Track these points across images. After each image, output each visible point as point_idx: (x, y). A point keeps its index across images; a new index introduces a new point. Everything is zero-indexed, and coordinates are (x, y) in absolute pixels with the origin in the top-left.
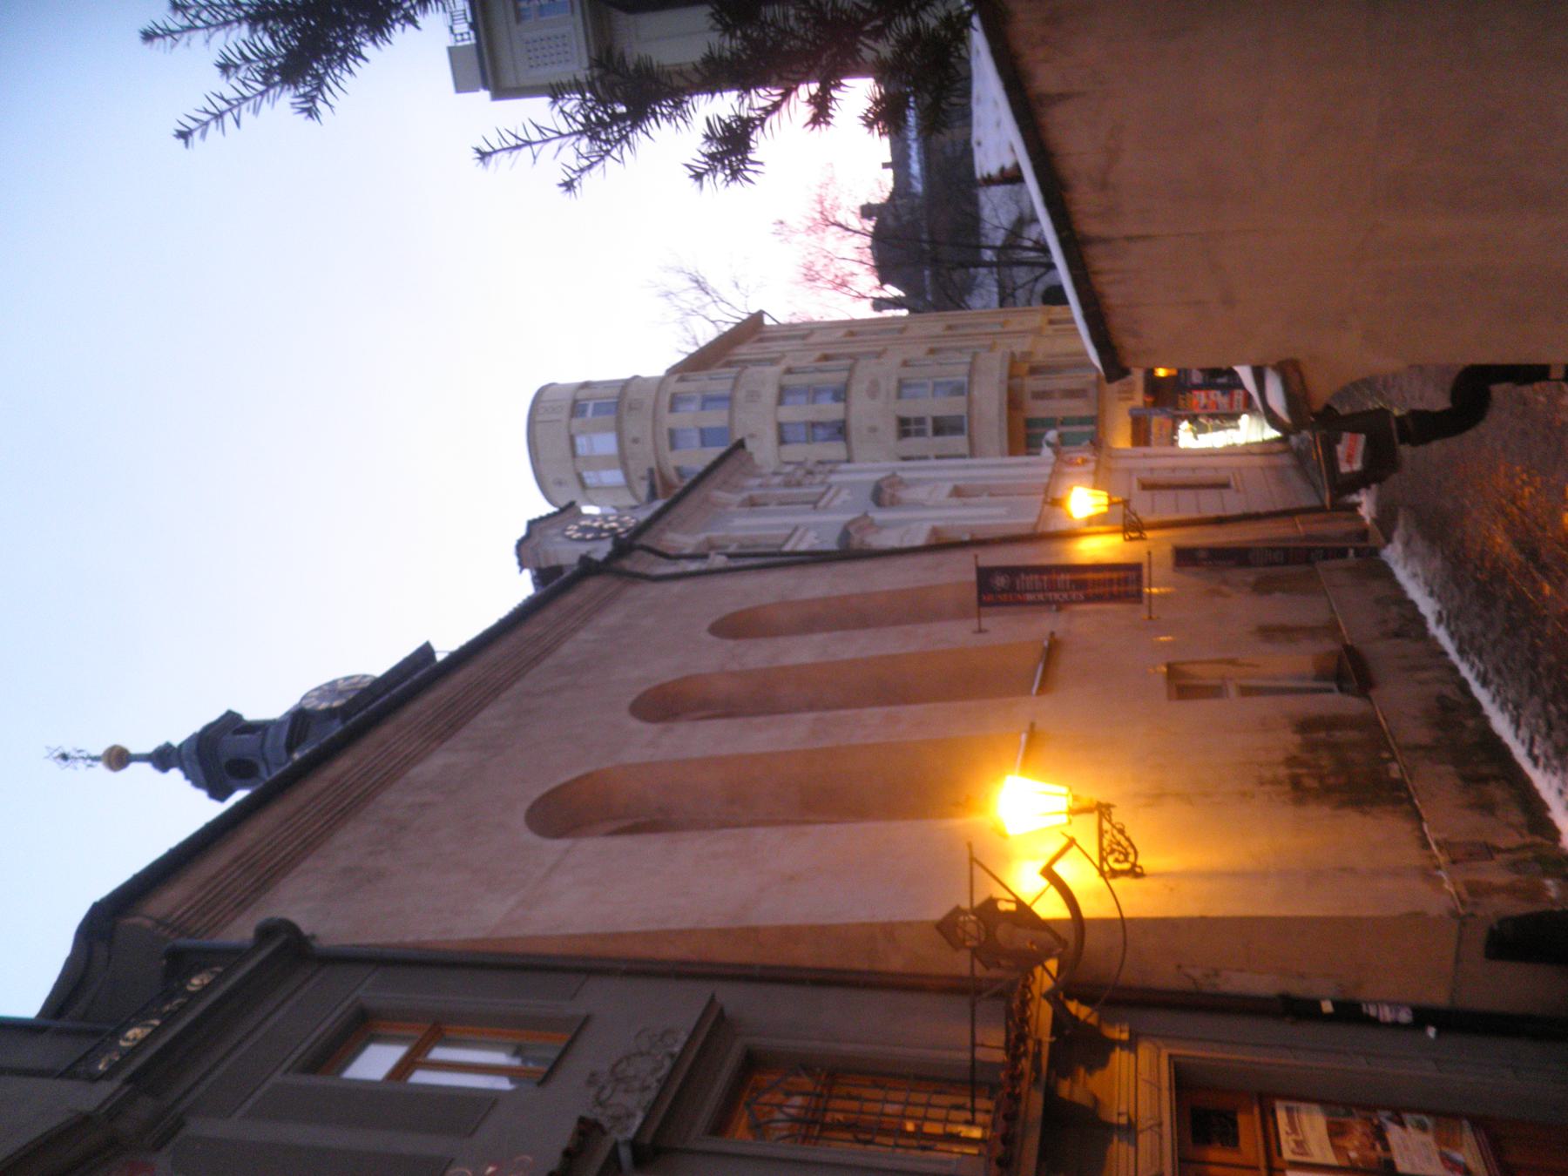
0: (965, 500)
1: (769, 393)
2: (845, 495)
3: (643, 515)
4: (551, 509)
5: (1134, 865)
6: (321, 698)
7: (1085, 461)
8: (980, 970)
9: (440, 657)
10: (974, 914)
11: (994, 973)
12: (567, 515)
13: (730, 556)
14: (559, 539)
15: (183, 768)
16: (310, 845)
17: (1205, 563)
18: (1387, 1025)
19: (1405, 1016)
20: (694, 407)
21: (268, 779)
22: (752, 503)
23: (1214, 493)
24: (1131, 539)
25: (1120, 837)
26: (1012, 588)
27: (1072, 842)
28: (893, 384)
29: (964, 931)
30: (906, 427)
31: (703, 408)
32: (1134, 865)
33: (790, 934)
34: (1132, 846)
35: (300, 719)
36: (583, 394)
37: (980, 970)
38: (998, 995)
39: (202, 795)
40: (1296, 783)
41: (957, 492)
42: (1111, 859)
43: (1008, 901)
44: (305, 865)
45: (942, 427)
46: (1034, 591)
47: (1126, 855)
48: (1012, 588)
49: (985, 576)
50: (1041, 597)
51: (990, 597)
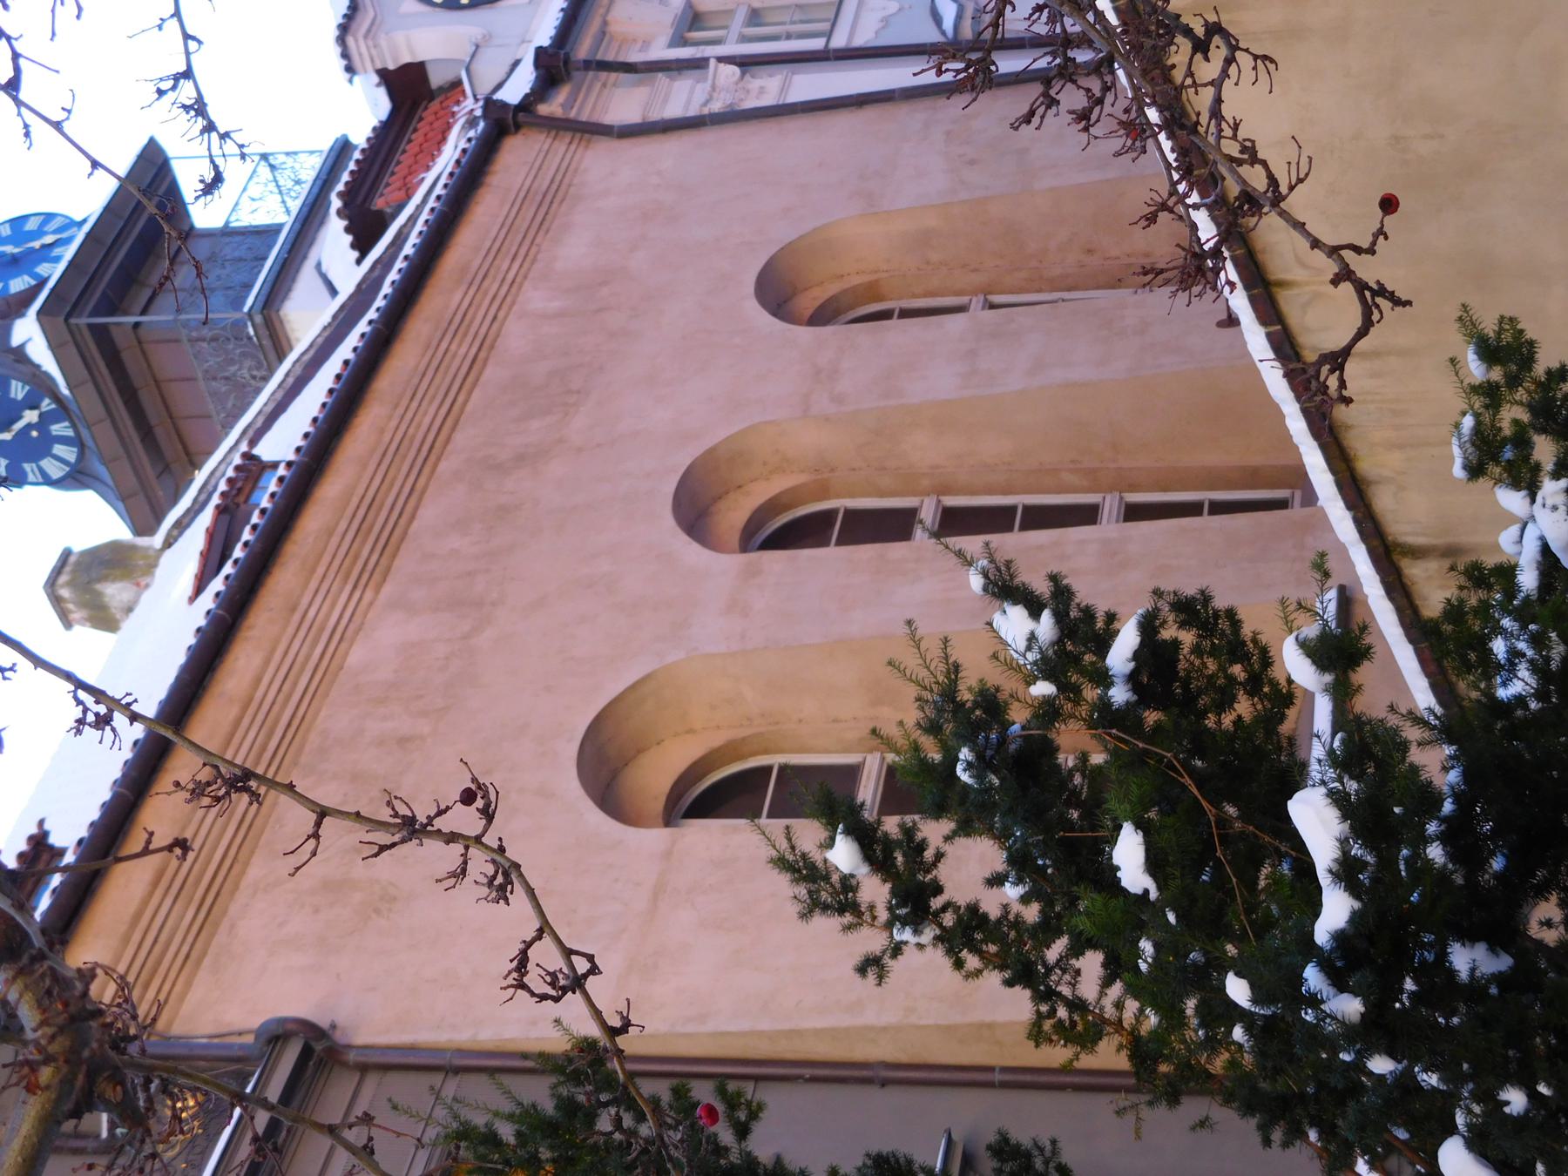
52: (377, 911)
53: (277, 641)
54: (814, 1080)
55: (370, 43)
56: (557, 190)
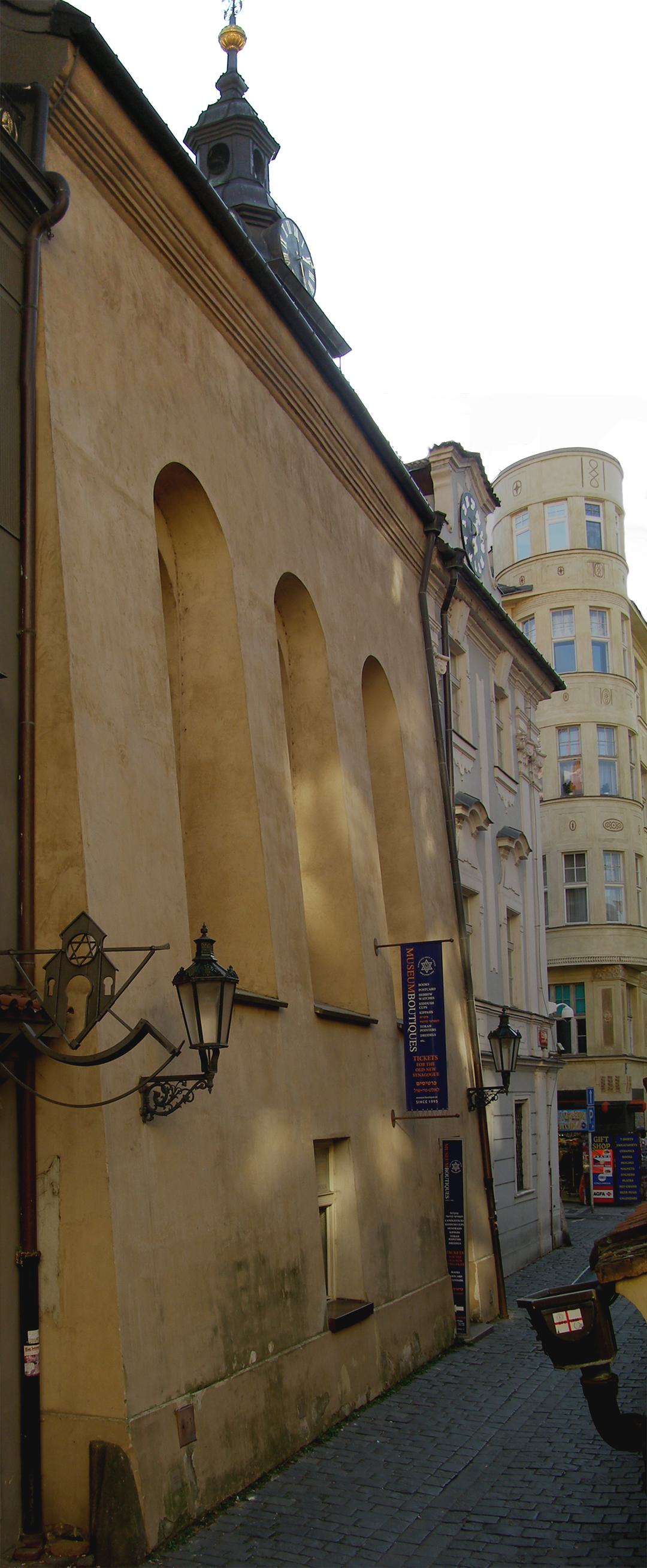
0: (504, 927)
1: (609, 715)
2: (509, 798)
3: (487, 583)
4: (491, 479)
5: (153, 1112)
6: (292, 240)
7: (543, 1045)
8: (42, 960)
9: (336, 361)
10: (98, 952)
11: (41, 974)
12: (486, 496)
13: (445, 677)
14: (461, 490)
15: (219, 102)
16: (141, 228)
17: (447, 1169)
18: (22, 1352)
19: (30, 1368)
20: (597, 635)
21: (211, 184)
22: (500, 695)
23: (514, 1176)
24: (469, 1096)
25: (180, 1097)
26: (419, 979)
27: (175, 1053)
28: (618, 847)
29: (80, 943)
30: (575, 859)
31: (594, 643)
32: (153, 1112)
33: (66, 757)
34: (171, 1111)
35: (271, 218)
36: (610, 508)
37: (42, 960)
38: (20, 978)
39: (193, 122)
40: (240, 1265)
41: (512, 915)
42: (158, 1089)
43: (113, 987)
44: (122, 225)
45: (576, 896)
46: (417, 1000)
47: (163, 1105)
48: (419, 979)
49: (433, 949)
50: (412, 1008)
51: (410, 955)
52: (106, 294)
53: (234, 288)
54: (22, 580)
55: (447, 461)
56: (304, 387)
